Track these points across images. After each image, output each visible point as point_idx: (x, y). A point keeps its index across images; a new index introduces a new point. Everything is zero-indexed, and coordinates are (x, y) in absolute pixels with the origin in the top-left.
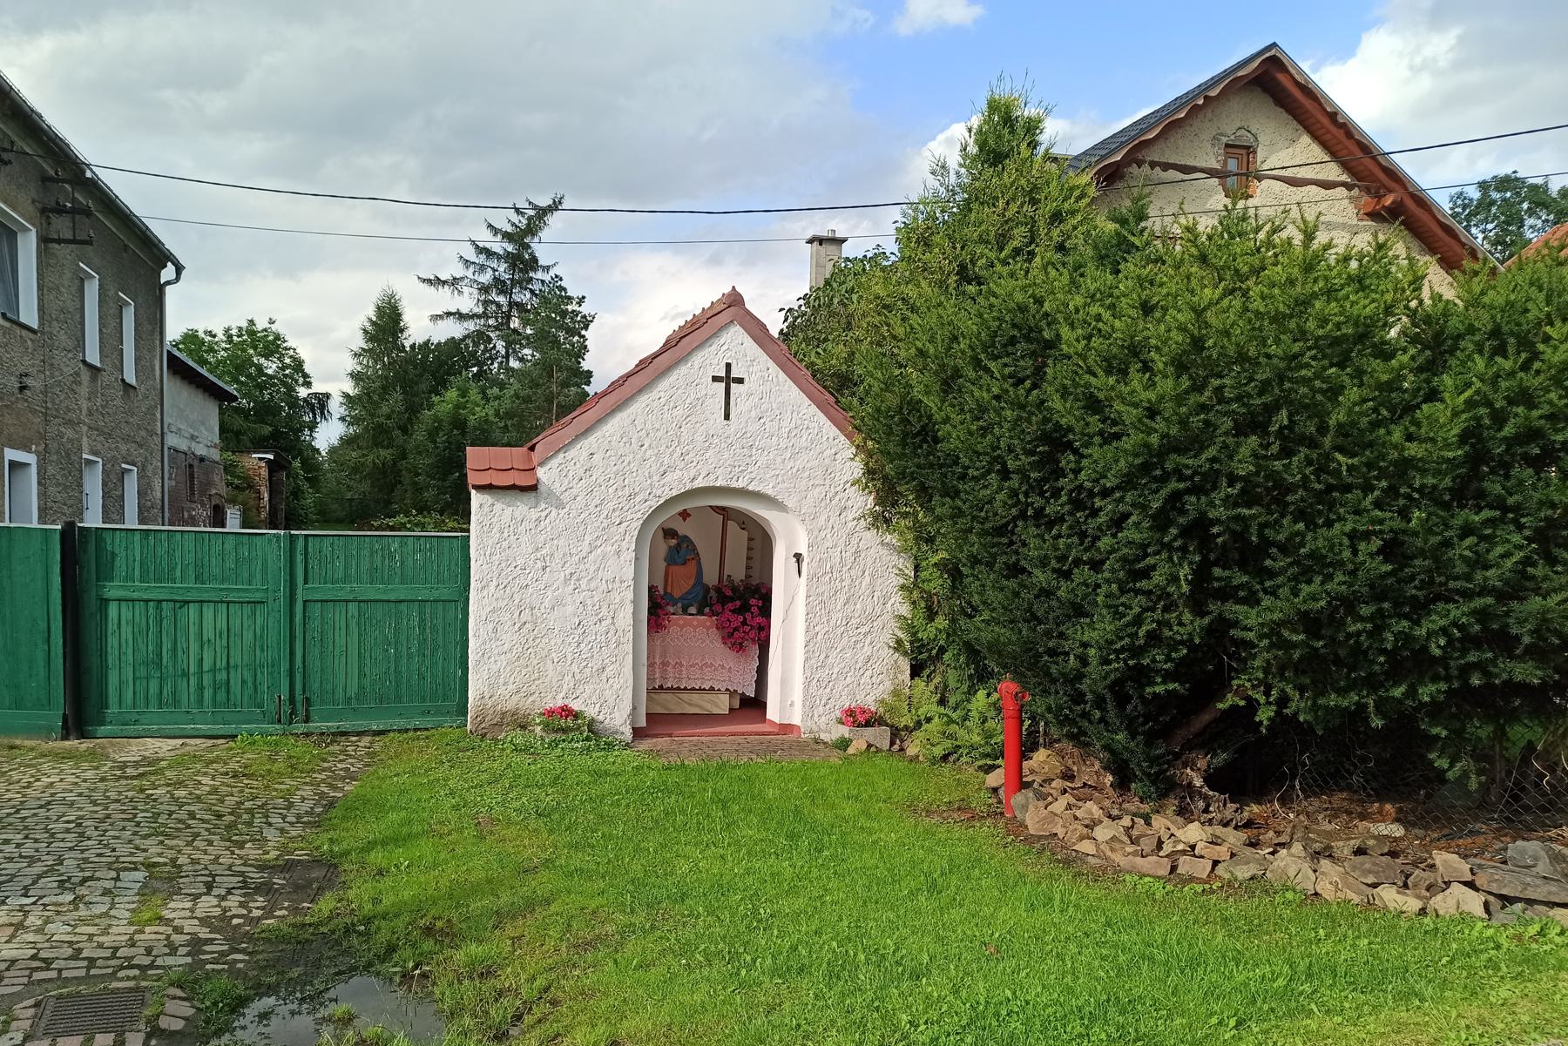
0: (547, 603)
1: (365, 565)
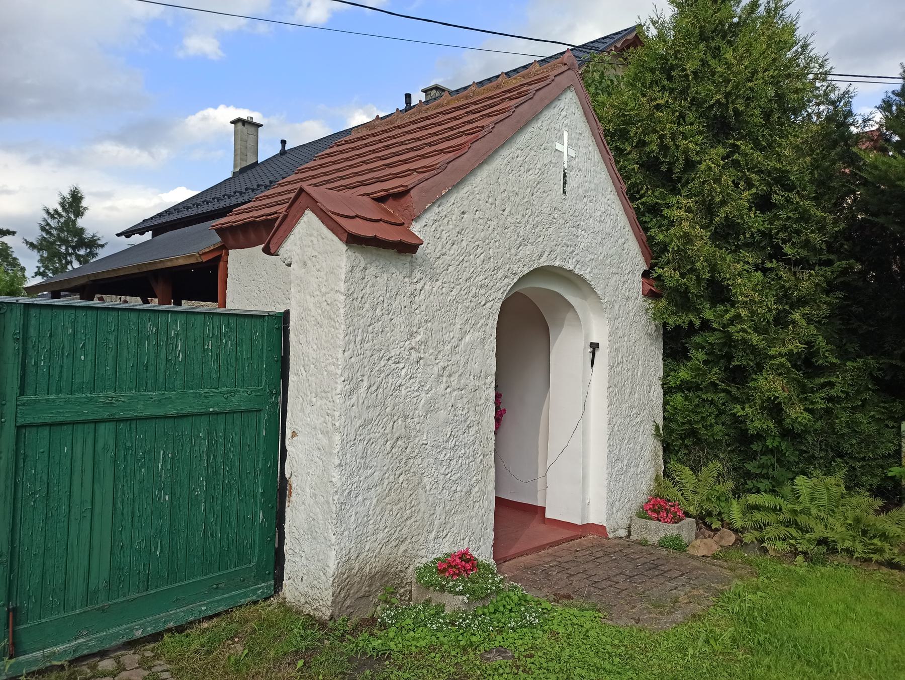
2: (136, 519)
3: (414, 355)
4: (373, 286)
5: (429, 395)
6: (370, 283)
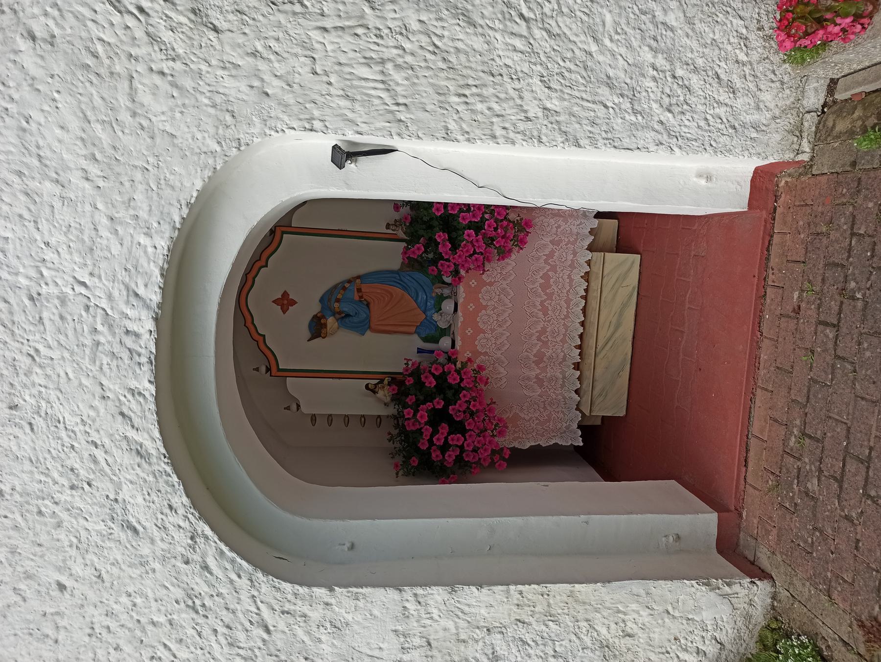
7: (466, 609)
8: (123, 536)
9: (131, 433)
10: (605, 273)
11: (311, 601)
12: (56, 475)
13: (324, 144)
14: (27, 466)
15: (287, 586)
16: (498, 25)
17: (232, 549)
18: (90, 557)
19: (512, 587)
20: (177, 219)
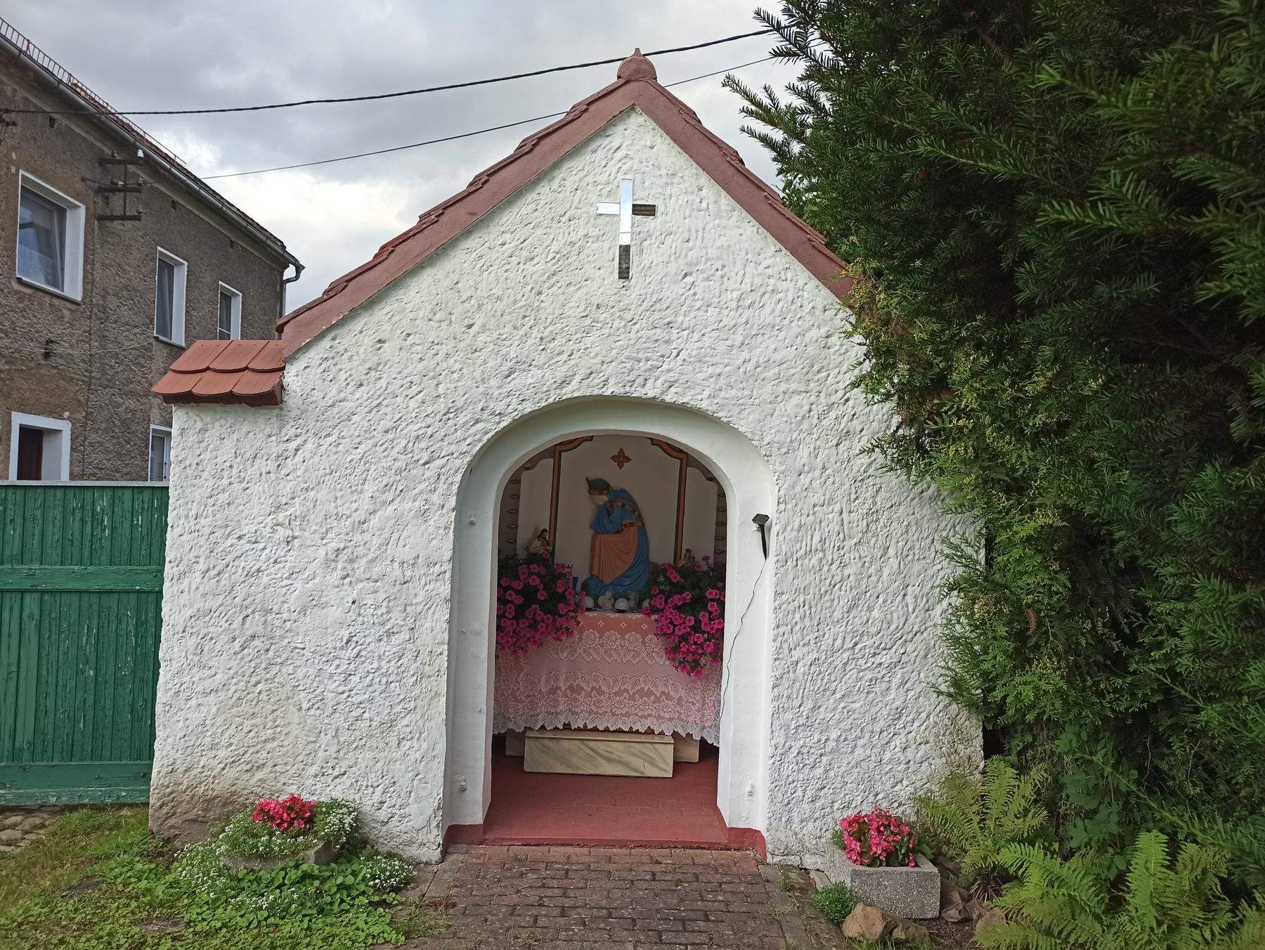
0: (293, 602)
1: (53, 533)
2: (60, 689)
3: (282, 533)
4: (216, 449)
5: (309, 586)
6: (212, 447)
7: (431, 611)
8: (504, 368)
9: (577, 378)
10: (657, 746)
11: (446, 495)
12: (550, 328)
13: (769, 509)
14: (558, 312)
15: (458, 478)
16: (849, 628)
17: (489, 440)
18: (492, 346)
19: (446, 647)
20: (719, 415)
